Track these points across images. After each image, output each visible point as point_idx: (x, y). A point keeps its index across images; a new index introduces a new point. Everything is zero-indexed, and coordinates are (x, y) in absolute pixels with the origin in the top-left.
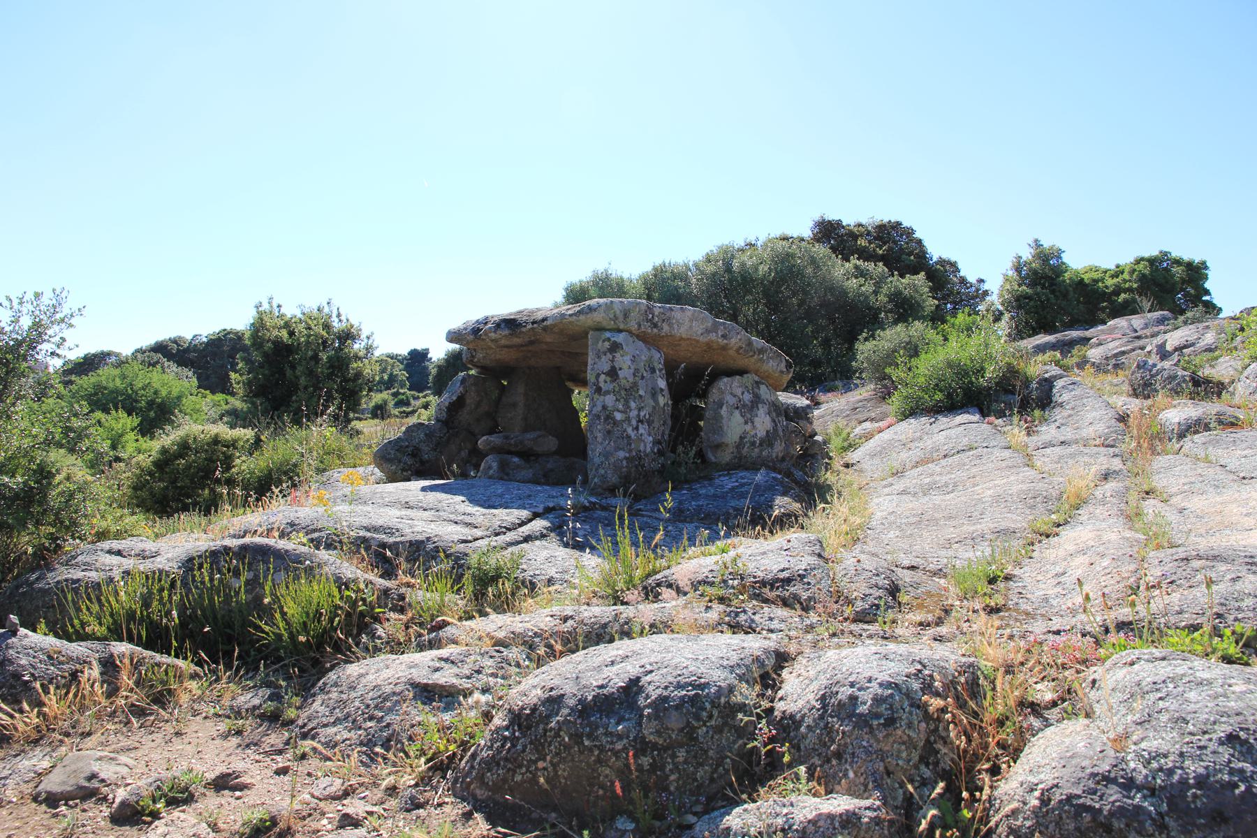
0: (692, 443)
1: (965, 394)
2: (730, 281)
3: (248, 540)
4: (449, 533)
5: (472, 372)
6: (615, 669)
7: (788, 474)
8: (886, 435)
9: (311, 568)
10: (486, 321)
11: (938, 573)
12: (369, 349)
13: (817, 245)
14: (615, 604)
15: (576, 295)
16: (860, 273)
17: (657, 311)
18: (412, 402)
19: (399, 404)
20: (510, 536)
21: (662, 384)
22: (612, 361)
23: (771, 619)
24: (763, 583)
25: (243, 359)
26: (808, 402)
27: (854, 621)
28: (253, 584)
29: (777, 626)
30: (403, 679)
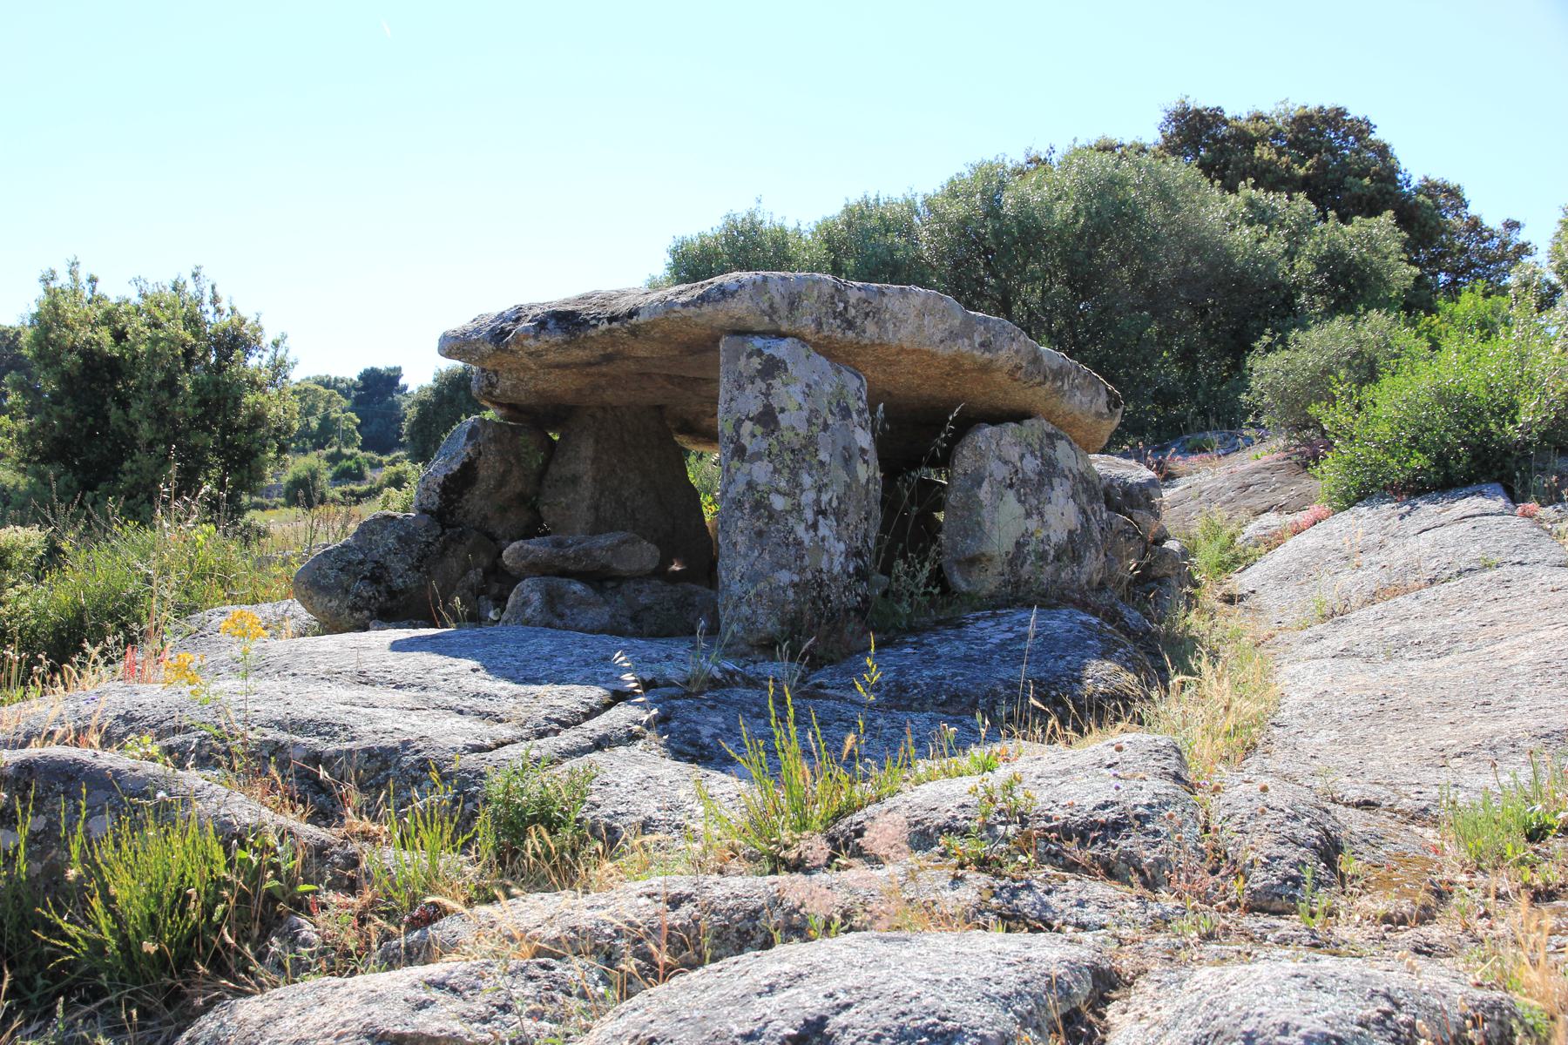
0: (923, 555)
1: (1474, 458)
2: (997, 234)
3: (34, 751)
4: (447, 733)
5: (490, 415)
6: (776, 1000)
7: (1112, 616)
8: (1309, 539)
9: (168, 807)
10: (518, 315)
11: (1420, 816)
12: (279, 367)
13: (1172, 160)
14: (774, 871)
15: (692, 264)
16: (1259, 216)
17: (853, 297)
18: (368, 472)
19: (343, 476)
20: (567, 738)
21: (864, 439)
22: (767, 395)
23: (1081, 904)
24: (1066, 832)
25: (18, 386)
26: (1151, 474)
27: (1250, 909)
28: (44, 841)
29: (1094, 919)
30: (354, 1027)
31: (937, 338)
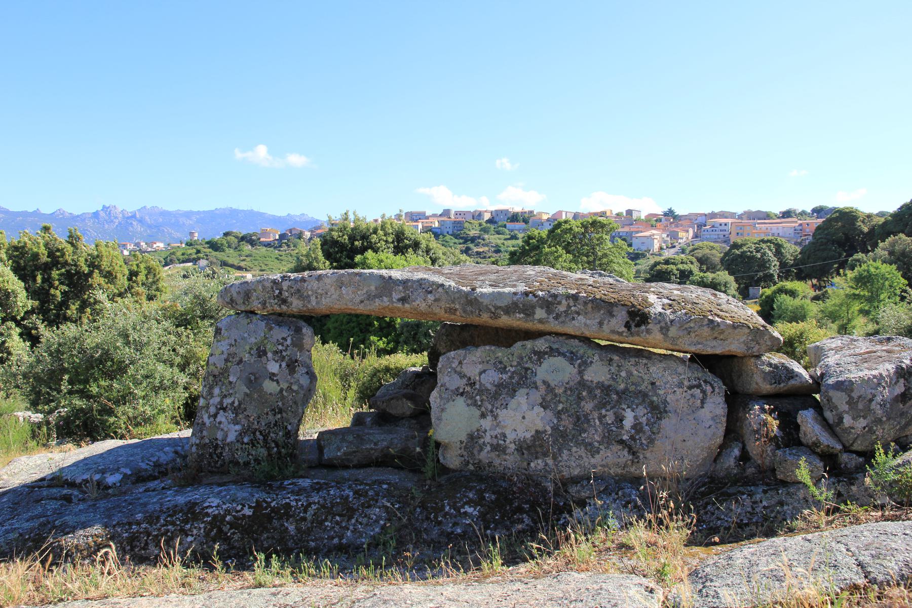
31: (358, 299)
